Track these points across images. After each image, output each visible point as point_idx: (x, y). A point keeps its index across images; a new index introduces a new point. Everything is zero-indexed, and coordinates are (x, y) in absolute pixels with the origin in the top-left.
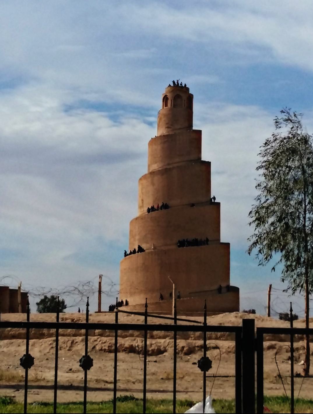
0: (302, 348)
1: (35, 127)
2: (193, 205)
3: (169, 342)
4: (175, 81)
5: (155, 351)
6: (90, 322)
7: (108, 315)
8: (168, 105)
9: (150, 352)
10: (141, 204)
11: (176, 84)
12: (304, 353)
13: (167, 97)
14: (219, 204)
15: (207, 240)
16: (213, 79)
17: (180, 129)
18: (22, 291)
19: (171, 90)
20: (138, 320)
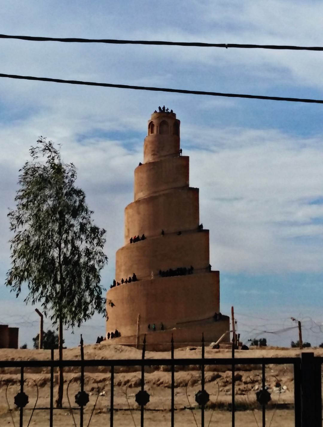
0: (109, 379)
2: (180, 233)
6: (86, 358)
8: (154, 132)
10: (127, 235)
11: (162, 110)
12: (251, 379)
13: (153, 124)
14: (207, 231)
15: (192, 268)
17: (165, 156)
19: (158, 116)
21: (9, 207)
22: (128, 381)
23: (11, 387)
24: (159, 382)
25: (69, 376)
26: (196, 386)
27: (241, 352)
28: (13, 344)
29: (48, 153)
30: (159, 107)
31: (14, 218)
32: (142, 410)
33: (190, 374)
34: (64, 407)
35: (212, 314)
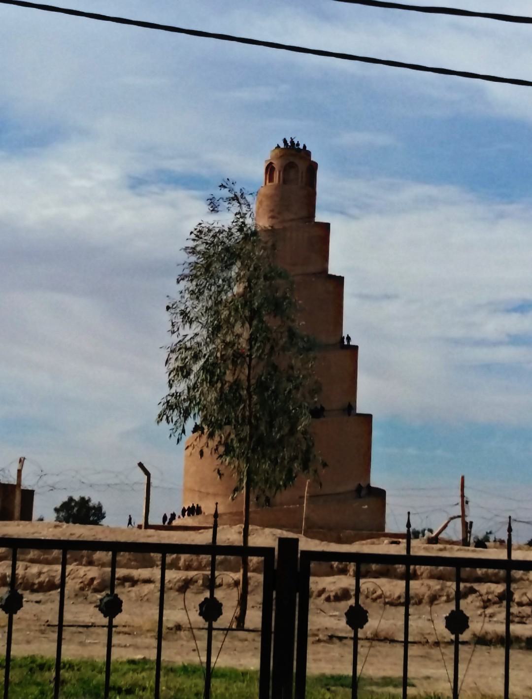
1: (79, 213)
3: (72, 570)
4: (287, 139)
5: (45, 584)
7: (22, 524)
9: (36, 587)
11: (289, 144)
14: (356, 348)
16: (383, 139)
17: (292, 220)
18: (22, 488)
19: (281, 154)
20: (71, 534)
21: (167, 295)
22: (323, 591)
23: (130, 589)
24: (375, 595)
25: (80, 573)
26: (437, 604)
27: (481, 551)
28: (26, 514)
29: (235, 207)
30: (283, 138)
31: (177, 313)
32: (456, 643)
33: (425, 584)
34: (247, 629)
35: (351, 486)
